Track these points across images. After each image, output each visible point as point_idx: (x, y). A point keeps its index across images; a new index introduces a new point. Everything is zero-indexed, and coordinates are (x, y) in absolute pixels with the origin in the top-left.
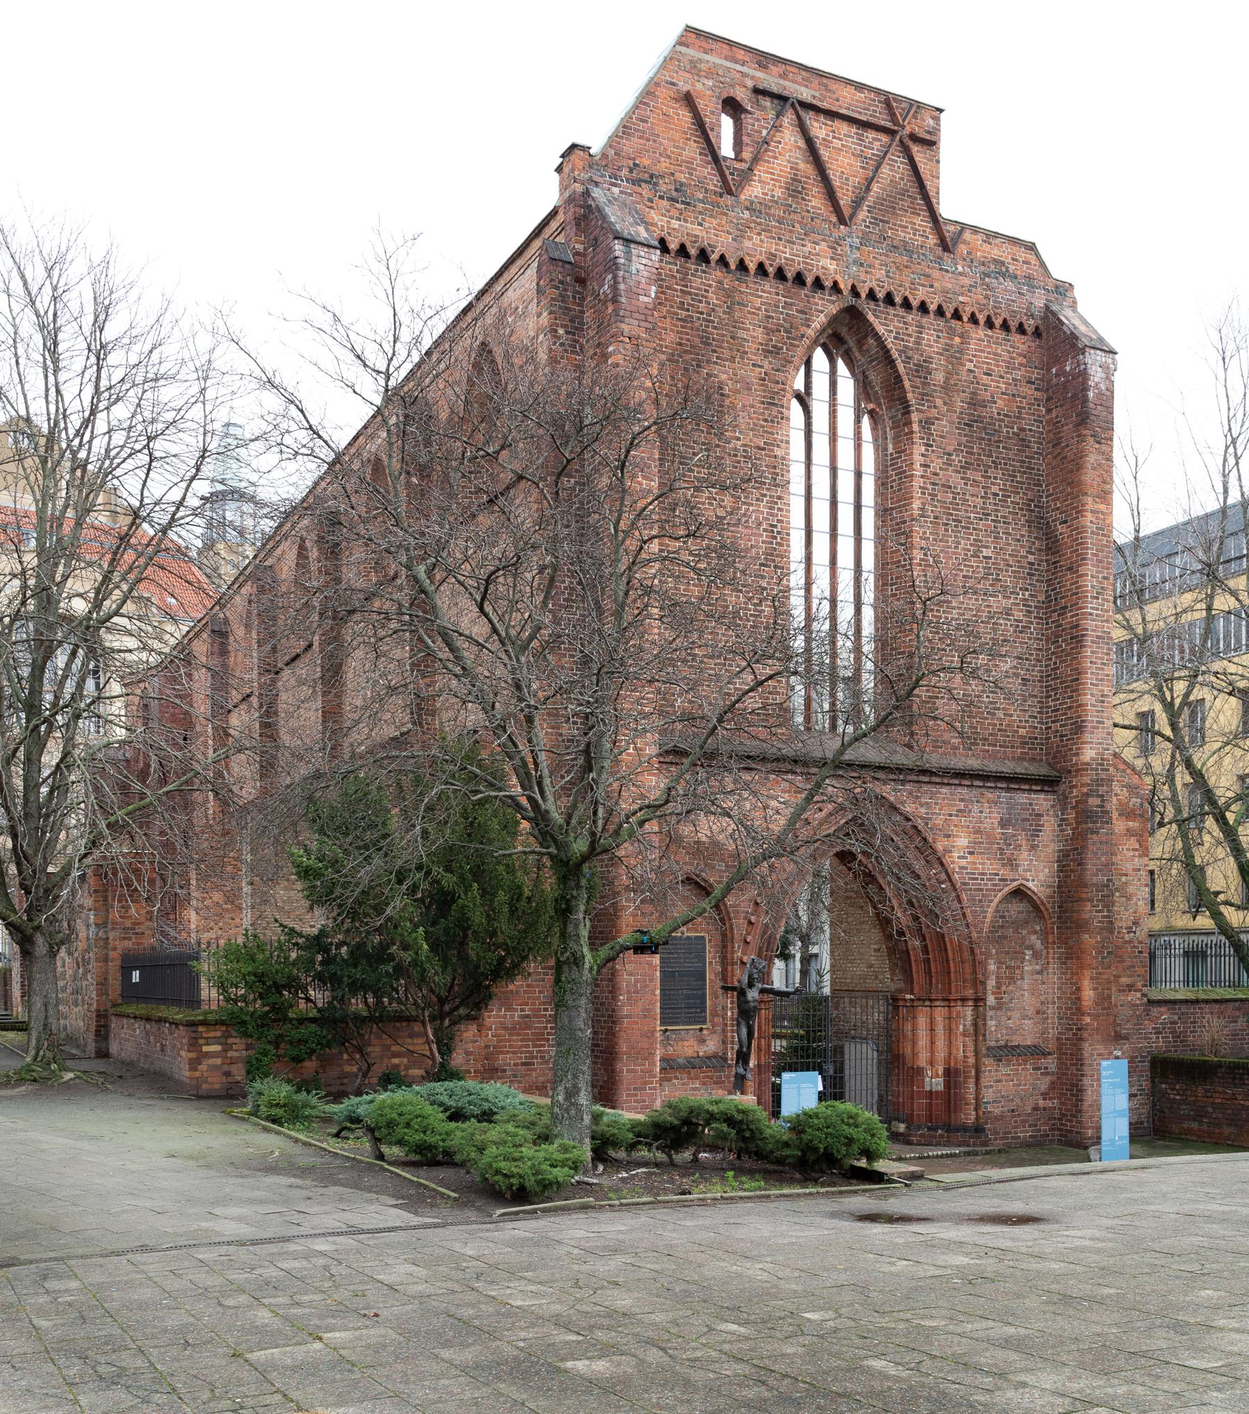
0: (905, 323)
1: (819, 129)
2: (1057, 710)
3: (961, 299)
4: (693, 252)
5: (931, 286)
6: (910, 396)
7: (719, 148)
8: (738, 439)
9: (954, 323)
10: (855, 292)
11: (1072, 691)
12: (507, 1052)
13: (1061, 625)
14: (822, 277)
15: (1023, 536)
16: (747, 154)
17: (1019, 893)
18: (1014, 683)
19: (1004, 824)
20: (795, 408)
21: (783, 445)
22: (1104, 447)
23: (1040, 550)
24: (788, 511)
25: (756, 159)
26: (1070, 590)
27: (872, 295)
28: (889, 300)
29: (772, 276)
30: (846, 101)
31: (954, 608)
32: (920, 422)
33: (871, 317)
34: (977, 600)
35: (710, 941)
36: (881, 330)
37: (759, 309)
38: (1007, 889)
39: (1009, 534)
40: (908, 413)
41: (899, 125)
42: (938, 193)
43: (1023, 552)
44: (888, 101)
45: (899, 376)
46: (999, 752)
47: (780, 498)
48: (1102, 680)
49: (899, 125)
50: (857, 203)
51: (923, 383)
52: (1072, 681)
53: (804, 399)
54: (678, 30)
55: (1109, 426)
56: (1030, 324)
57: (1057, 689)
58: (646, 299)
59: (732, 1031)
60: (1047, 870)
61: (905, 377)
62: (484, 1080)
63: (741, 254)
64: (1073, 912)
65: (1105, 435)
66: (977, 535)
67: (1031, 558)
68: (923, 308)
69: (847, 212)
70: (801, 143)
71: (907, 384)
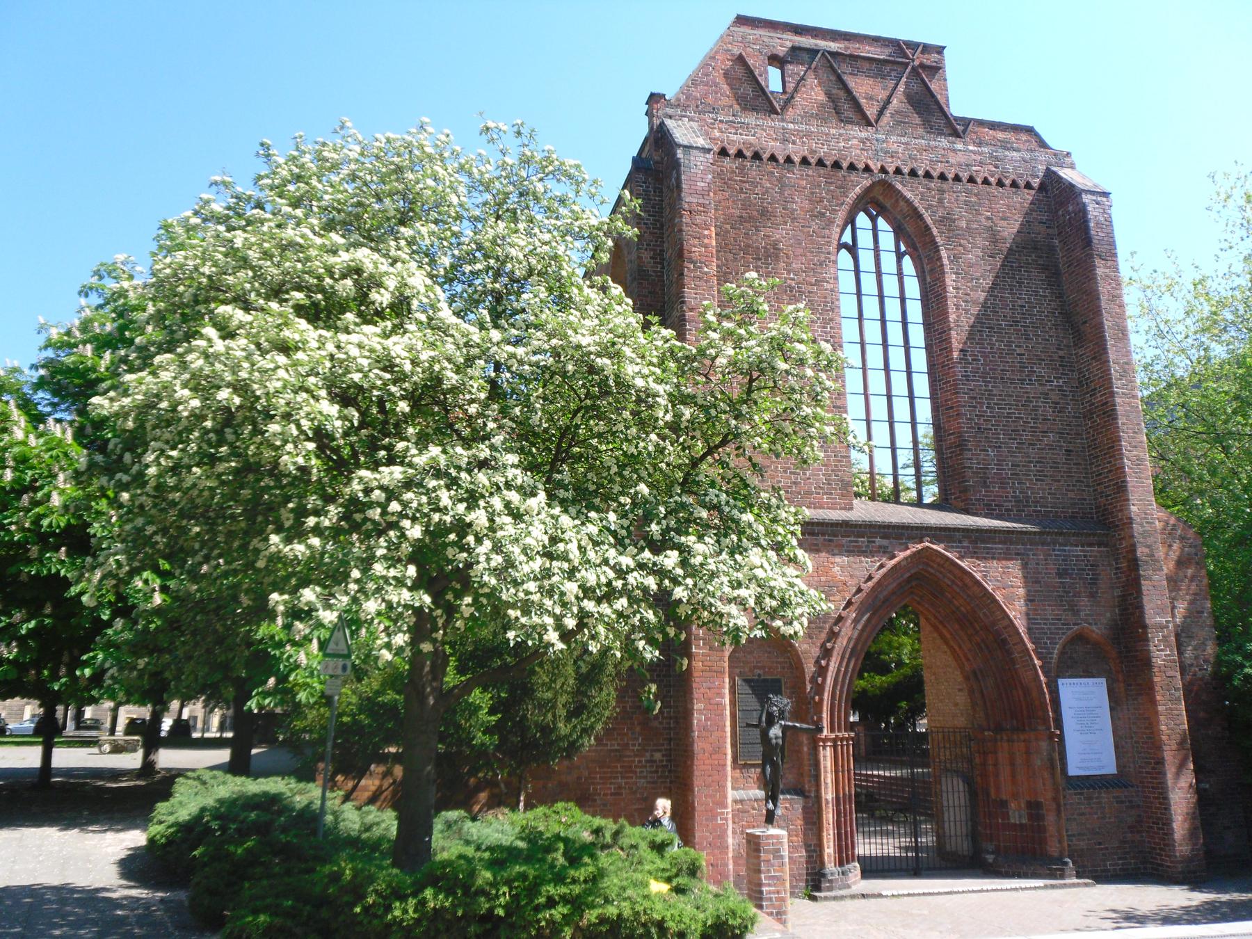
0: (928, 189)
1: (843, 69)
2: (1100, 474)
3: (974, 168)
4: (748, 154)
5: (947, 162)
6: (938, 239)
7: (948, 106)
8: (793, 279)
9: (969, 186)
10: (883, 170)
11: (1110, 457)
12: (599, 783)
13: (1093, 404)
14: (856, 162)
15: (1050, 336)
16: (790, 86)
17: (1080, 638)
18: (1058, 454)
19: (1059, 575)
20: (844, 258)
21: (832, 281)
22: (1109, 263)
23: (1068, 346)
24: (840, 329)
25: (796, 90)
26: (1097, 375)
27: (898, 171)
28: (913, 173)
29: (798, 164)
30: (868, 51)
31: (995, 395)
32: (949, 257)
33: (899, 186)
34: (1015, 388)
35: (786, 683)
36: (909, 195)
37: (805, 188)
38: (1069, 632)
39: (1039, 336)
40: (938, 251)
41: (909, 58)
42: (948, 100)
43: (1053, 349)
44: (896, 45)
45: (927, 226)
46: (1051, 512)
47: (831, 320)
48: (1135, 447)
49: (909, 58)
50: (881, 113)
51: (949, 230)
52: (1109, 448)
53: (853, 249)
54: (732, 17)
55: (1112, 244)
56: (1036, 183)
57: (1098, 456)
58: (703, 184)
59: (810, 765)
60: (1108, 615)
61: (932, 226)
62: (19, 407)
63: (787, 152)
64: (1137, 651)
65: (1111, 254)
66: (1010, 338)
67: (1061, 353)
68: (942, 177)
69: (872, 117)
70: (833, 78)
71: (935, 231)
